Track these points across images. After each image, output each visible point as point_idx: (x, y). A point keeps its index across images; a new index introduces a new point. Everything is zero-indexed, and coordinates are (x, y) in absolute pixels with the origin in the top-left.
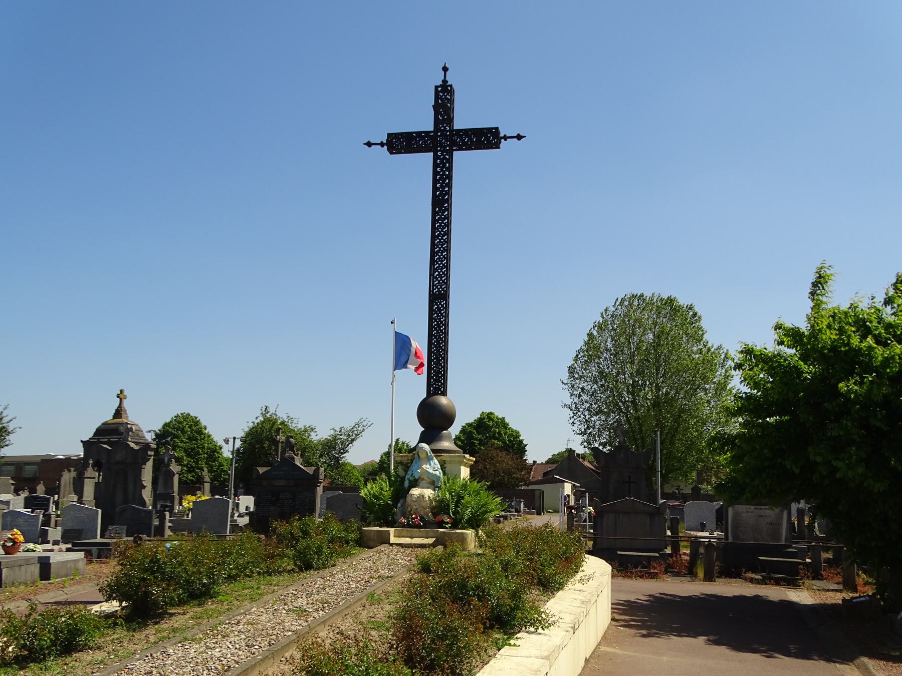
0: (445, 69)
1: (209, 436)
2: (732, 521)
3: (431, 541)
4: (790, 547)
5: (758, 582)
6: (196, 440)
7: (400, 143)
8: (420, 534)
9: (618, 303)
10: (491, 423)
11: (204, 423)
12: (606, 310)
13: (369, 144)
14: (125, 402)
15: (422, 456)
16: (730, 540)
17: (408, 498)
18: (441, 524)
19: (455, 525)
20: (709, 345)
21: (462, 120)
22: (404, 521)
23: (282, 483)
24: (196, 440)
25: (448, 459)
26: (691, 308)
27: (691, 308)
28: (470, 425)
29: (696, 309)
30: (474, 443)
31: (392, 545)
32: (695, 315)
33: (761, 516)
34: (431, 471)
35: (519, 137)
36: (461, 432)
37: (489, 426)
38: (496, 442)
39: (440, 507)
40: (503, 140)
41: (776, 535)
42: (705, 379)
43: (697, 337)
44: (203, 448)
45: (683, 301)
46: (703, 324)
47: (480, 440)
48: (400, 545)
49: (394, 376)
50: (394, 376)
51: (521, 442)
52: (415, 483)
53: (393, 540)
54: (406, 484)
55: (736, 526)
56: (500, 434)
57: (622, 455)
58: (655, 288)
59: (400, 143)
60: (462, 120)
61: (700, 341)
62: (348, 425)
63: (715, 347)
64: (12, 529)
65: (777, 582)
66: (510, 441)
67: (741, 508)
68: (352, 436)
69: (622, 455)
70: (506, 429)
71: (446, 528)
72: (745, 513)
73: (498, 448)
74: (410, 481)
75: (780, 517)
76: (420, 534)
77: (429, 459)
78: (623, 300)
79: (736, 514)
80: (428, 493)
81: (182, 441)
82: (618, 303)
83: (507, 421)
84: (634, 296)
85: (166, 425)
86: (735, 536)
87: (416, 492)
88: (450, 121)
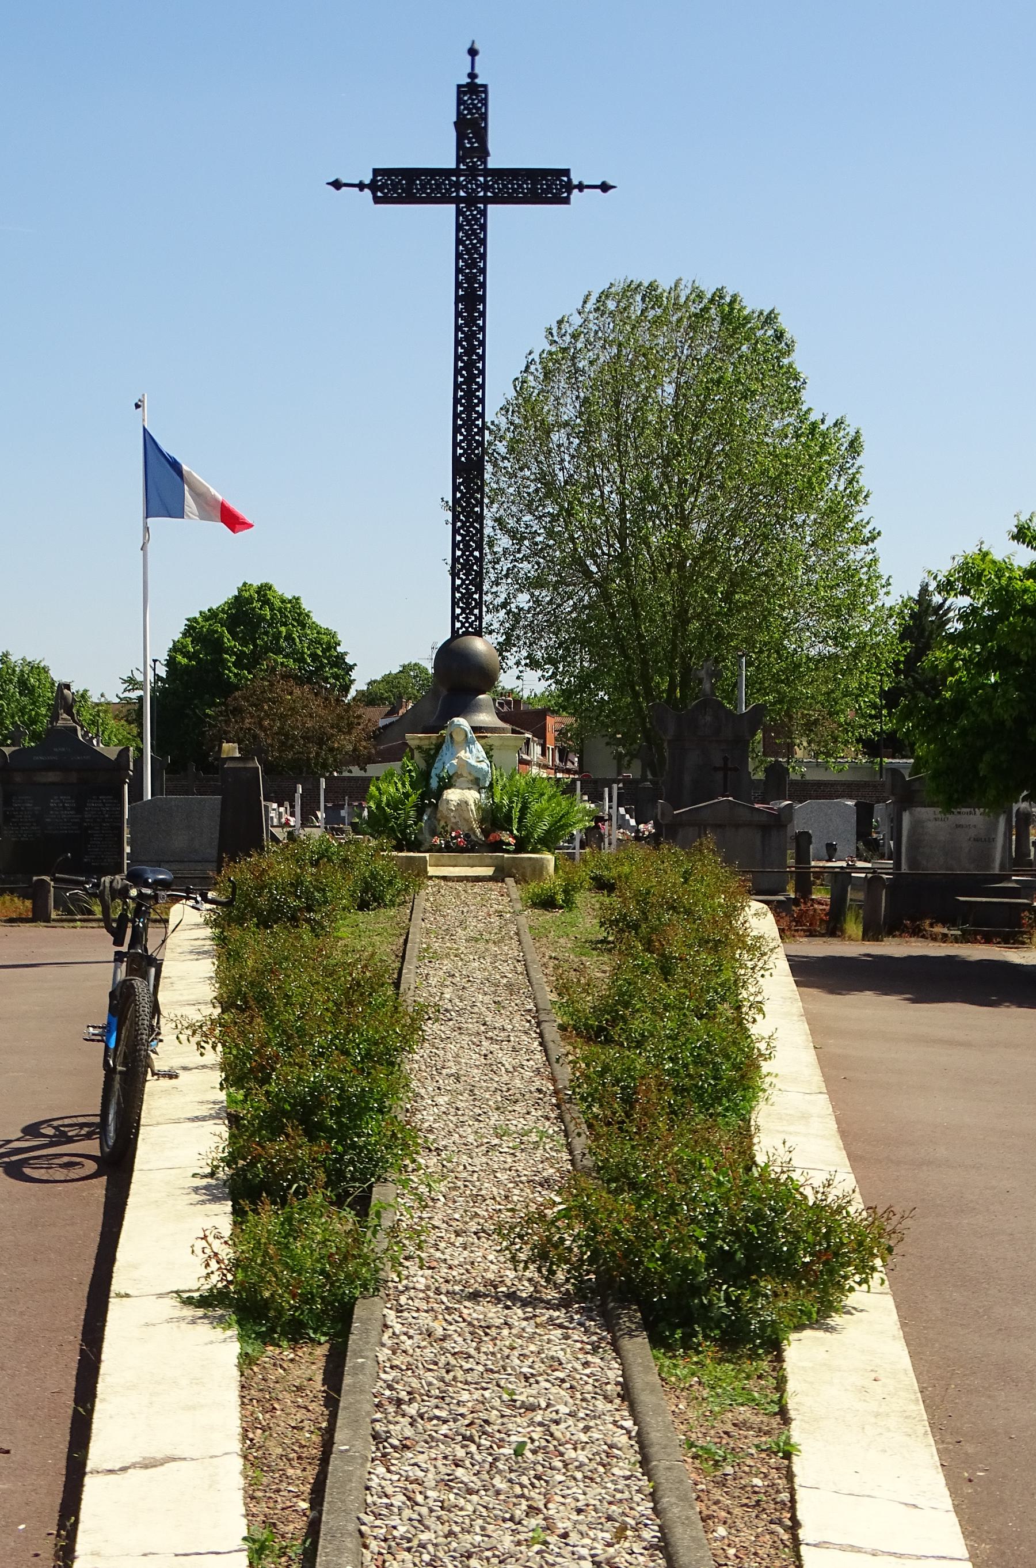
0: (473, 52)
2: (909, 837)
3: (489, 871)
4: (1009, 880)
5: (956, 940)
7: (396, 186)
8: (471, 862)
9: (590, 306)
10: (267, 612)
12: (560, 322)
13: (337, 185)
15: (458, 738)
16: (904, 868)
17: (442, 807)
18: (498, 846)
19: (520, 847)
20: (813, 417)
22: (437, 841)
25: (496, 743)
26: (770, 319)
27: (770, 319)
28: (212, 615)
29: (784, 322)
30: (224, 662)
31: (431, 878)
32: (779, 336)
33: (958, 826)
34: (473, 762)
35: (605, 187)
36: (185, 635)
38: (280, 659)
39: (494, 818)
40: (576, 191)
41: (985, 858)
43: (788, 389)
45: (752, 303)
46: (799, 360)
47: (240, 656)
48: (445, 878)
49: (147, 529)
50: (147, 529)
51: (341, 657)
52: (448, 783)
53: (432, 871)
54: (434, 783)
55: (915, 845)
56: (289, 638)
57: (708, 718)
59: (396, 186)
63: (829, 422)
65: (988, 940)
66: (314, 657)
67: (925, 813)
69: (708, 718)
70: (303, 626)
71: (508, 852)
72: (929, 819)
74: (441, 779)
75: (993, 827)
76: (471, 862)
77: (468, 742)
78: (605, 295)
79: (916, 825)
80: (472, 796)
82: (590, 306)
83: (306, 606)
84: (631, 289)
86: (913, 863)
87: (453, 795)
88: (483, 153)
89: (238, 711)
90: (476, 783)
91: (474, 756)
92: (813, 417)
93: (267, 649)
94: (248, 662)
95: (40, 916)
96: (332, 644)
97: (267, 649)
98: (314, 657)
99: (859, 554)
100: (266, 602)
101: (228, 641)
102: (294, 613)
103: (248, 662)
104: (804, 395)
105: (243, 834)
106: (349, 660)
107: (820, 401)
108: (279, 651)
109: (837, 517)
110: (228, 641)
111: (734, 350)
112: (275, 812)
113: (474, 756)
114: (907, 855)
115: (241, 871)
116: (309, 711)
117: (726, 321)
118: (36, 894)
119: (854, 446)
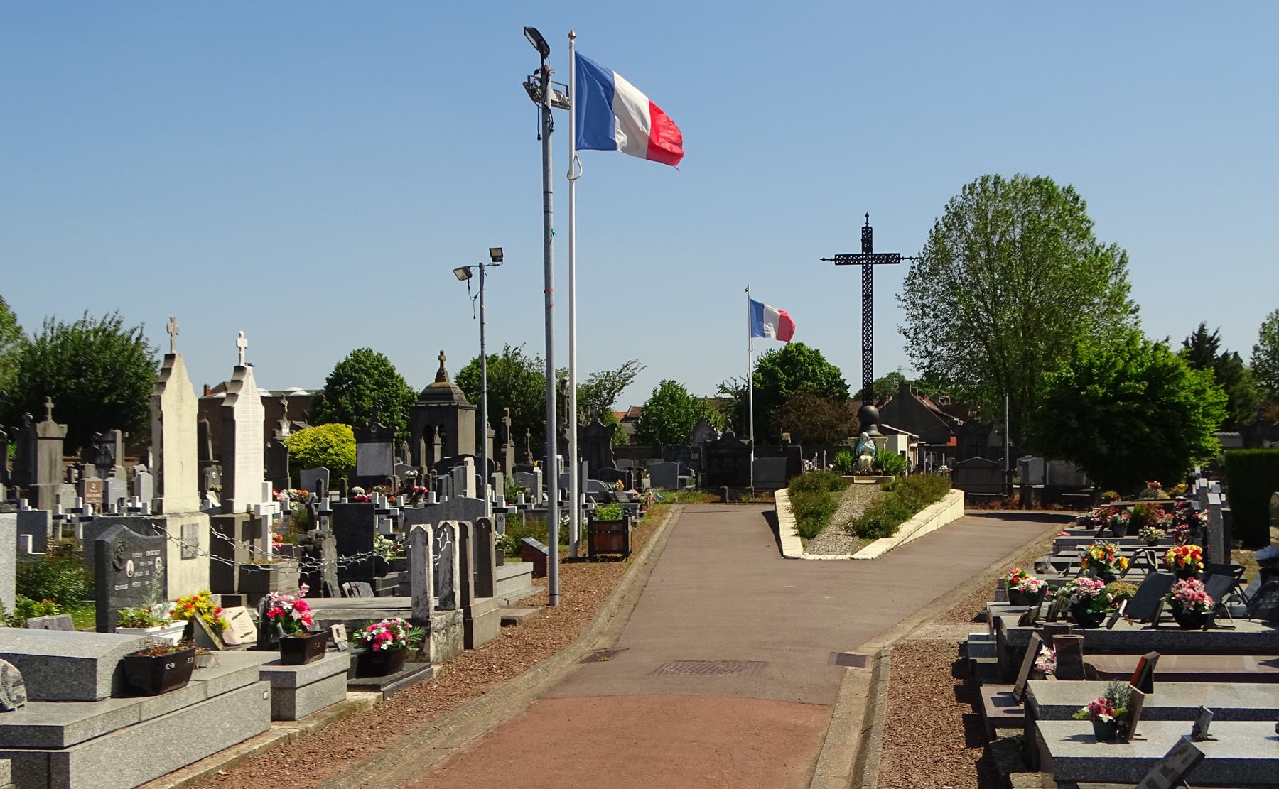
1: (402, 380)
6: (387, 386)
11: (392, 361)
12: (951, 201)
14: (445, 363)
20: (1097, 243)
21: (857, 249)
23: (724, 451)
24: (387, 386)
26: (1069, 190)
27: (1069, 190)
29: (1078, 192)
32: (1077, 199)
37: (799, 361)
39: (877, 465)
42: (1093, 291)
44: (397, 396)
45: (1060, 183)
46: (1089, 213)
55: (1052, 475)
56: (814, 370)
58: (1015, 165)
60: (857, 249)
61: (1084, 236)
62: (614, 367)
63: (1108, 246)
64: (615, 481)
68: (617, 383)
73: (815, 393)
80: (870, 458)
81: (368, 388)
83: (822, 354)
85: (340, 367)
87: (863, 457)
89: (787, 412)
90: (871, 454)
91: (870, 445)
92: (1097, 243)
93: (802, 378)
94: (792, 386)
95: (723, 501)
96: (837, 374)
97: (802, 378)
98: (827, 381)
99: (1129, 320)
100: (801, 353)
101: (781, 374)
102: (816, 358)
103: (792, 386)
104: (1093, 230)
105: (795, 469)
106: (846, 383)
107: (1103, 235)
108: (808, 379)
109: (1117, 298)
110: (781, 374)
111: (1051, 206)
112: (807, 464)
113: (870, 445)
114: (551, 421)
115: (795, 481)
116: (828, 412)
117: (1042, 190)
118: (722, 493)
119: (1123, 261)
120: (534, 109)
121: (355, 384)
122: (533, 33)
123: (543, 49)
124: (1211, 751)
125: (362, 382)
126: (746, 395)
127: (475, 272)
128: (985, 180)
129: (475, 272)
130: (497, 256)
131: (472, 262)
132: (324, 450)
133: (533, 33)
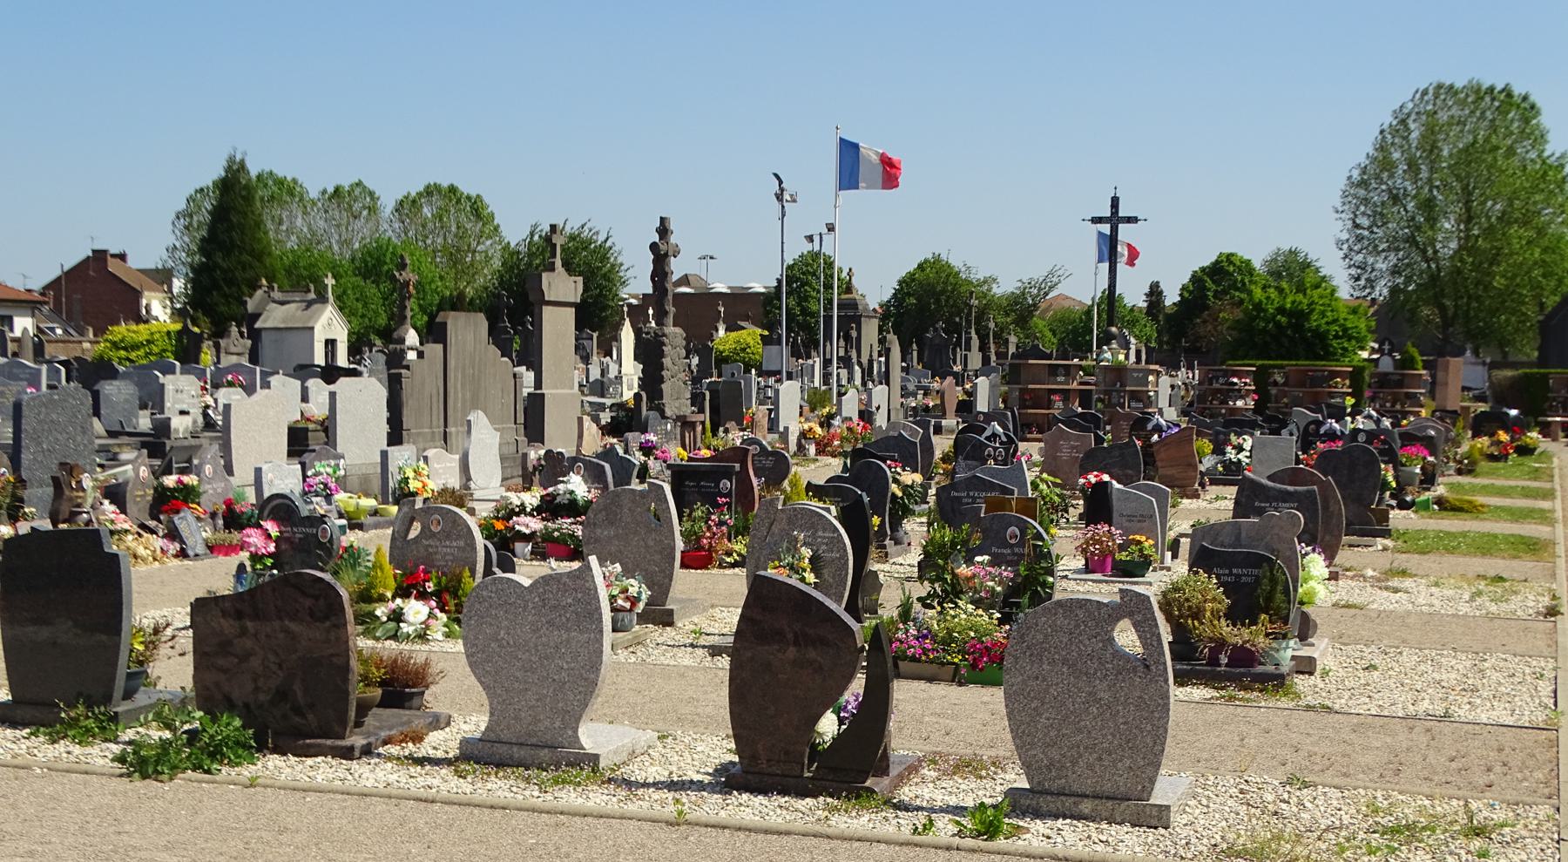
26: (1525, 98)
27: (1525, 98)
29: (1532, 98)
100: (1231, 263)
101: (1209, 283)
108: (1237, 289)
111: (1510, 112)
120: (777, 205)
121: (803, 285)
122: (776, 176)
123: (781, 182)
124: (1464, 663)
125: (807, 283)
126: (1089, 312)
127: (817, 239)
128: (1440, 86)
129: (817, 239)
130: (831, 228)
131: (815, 232)
132: (744, 350)
133: (776, 176)
